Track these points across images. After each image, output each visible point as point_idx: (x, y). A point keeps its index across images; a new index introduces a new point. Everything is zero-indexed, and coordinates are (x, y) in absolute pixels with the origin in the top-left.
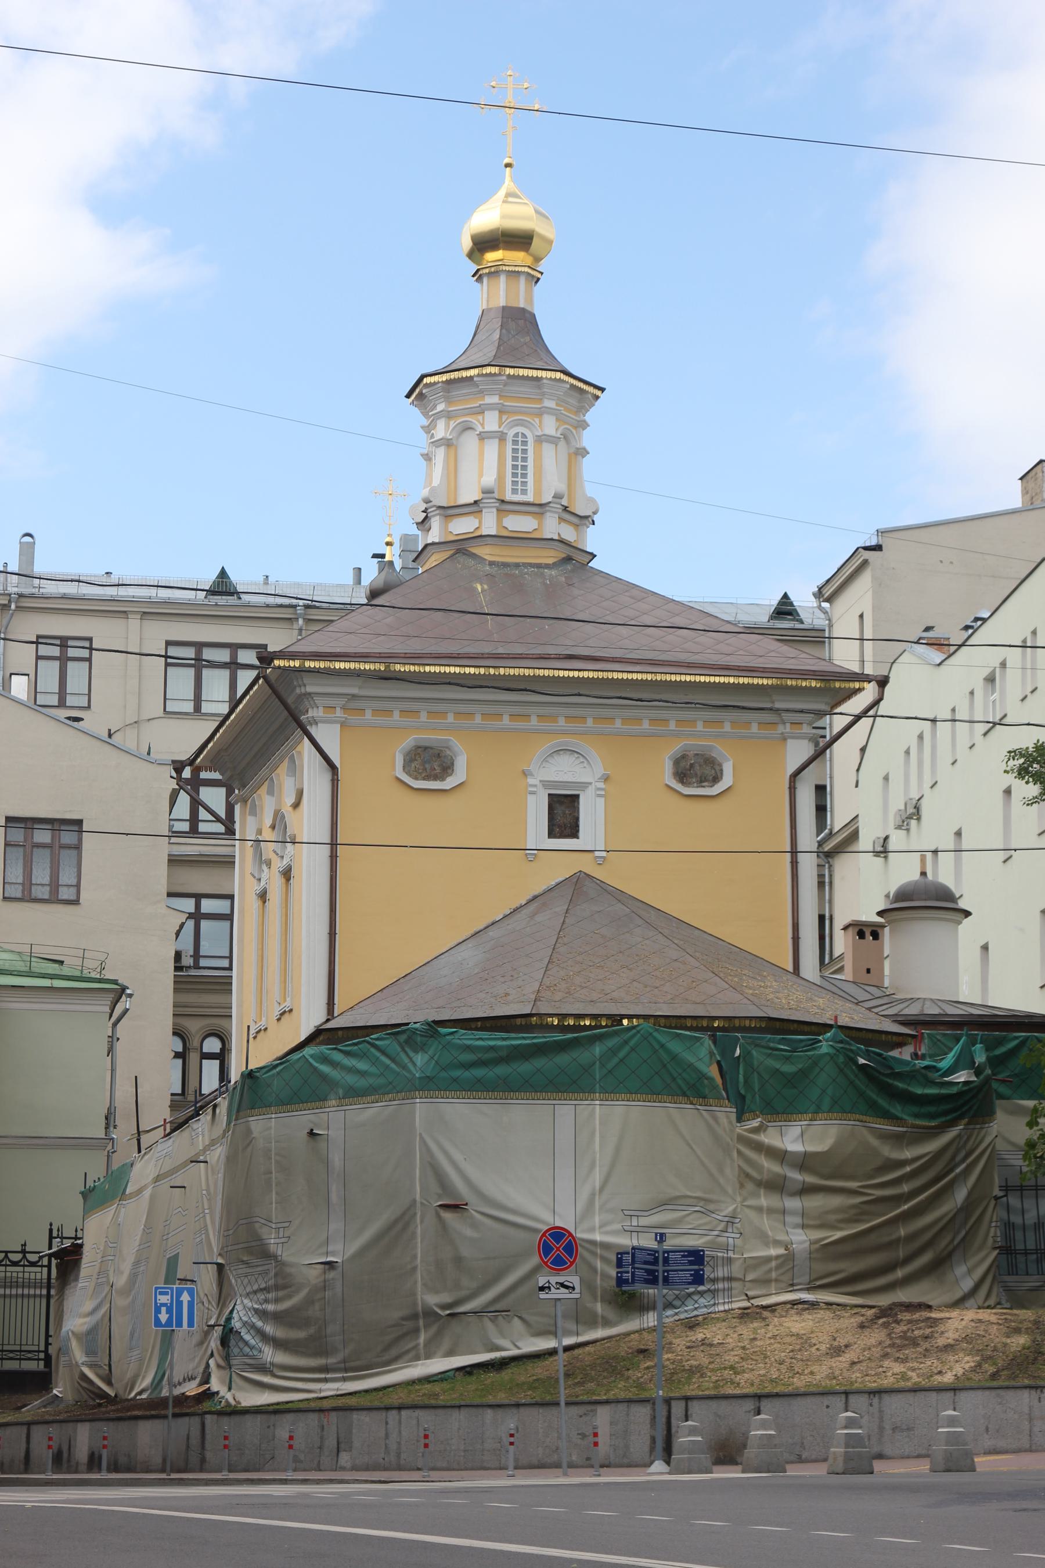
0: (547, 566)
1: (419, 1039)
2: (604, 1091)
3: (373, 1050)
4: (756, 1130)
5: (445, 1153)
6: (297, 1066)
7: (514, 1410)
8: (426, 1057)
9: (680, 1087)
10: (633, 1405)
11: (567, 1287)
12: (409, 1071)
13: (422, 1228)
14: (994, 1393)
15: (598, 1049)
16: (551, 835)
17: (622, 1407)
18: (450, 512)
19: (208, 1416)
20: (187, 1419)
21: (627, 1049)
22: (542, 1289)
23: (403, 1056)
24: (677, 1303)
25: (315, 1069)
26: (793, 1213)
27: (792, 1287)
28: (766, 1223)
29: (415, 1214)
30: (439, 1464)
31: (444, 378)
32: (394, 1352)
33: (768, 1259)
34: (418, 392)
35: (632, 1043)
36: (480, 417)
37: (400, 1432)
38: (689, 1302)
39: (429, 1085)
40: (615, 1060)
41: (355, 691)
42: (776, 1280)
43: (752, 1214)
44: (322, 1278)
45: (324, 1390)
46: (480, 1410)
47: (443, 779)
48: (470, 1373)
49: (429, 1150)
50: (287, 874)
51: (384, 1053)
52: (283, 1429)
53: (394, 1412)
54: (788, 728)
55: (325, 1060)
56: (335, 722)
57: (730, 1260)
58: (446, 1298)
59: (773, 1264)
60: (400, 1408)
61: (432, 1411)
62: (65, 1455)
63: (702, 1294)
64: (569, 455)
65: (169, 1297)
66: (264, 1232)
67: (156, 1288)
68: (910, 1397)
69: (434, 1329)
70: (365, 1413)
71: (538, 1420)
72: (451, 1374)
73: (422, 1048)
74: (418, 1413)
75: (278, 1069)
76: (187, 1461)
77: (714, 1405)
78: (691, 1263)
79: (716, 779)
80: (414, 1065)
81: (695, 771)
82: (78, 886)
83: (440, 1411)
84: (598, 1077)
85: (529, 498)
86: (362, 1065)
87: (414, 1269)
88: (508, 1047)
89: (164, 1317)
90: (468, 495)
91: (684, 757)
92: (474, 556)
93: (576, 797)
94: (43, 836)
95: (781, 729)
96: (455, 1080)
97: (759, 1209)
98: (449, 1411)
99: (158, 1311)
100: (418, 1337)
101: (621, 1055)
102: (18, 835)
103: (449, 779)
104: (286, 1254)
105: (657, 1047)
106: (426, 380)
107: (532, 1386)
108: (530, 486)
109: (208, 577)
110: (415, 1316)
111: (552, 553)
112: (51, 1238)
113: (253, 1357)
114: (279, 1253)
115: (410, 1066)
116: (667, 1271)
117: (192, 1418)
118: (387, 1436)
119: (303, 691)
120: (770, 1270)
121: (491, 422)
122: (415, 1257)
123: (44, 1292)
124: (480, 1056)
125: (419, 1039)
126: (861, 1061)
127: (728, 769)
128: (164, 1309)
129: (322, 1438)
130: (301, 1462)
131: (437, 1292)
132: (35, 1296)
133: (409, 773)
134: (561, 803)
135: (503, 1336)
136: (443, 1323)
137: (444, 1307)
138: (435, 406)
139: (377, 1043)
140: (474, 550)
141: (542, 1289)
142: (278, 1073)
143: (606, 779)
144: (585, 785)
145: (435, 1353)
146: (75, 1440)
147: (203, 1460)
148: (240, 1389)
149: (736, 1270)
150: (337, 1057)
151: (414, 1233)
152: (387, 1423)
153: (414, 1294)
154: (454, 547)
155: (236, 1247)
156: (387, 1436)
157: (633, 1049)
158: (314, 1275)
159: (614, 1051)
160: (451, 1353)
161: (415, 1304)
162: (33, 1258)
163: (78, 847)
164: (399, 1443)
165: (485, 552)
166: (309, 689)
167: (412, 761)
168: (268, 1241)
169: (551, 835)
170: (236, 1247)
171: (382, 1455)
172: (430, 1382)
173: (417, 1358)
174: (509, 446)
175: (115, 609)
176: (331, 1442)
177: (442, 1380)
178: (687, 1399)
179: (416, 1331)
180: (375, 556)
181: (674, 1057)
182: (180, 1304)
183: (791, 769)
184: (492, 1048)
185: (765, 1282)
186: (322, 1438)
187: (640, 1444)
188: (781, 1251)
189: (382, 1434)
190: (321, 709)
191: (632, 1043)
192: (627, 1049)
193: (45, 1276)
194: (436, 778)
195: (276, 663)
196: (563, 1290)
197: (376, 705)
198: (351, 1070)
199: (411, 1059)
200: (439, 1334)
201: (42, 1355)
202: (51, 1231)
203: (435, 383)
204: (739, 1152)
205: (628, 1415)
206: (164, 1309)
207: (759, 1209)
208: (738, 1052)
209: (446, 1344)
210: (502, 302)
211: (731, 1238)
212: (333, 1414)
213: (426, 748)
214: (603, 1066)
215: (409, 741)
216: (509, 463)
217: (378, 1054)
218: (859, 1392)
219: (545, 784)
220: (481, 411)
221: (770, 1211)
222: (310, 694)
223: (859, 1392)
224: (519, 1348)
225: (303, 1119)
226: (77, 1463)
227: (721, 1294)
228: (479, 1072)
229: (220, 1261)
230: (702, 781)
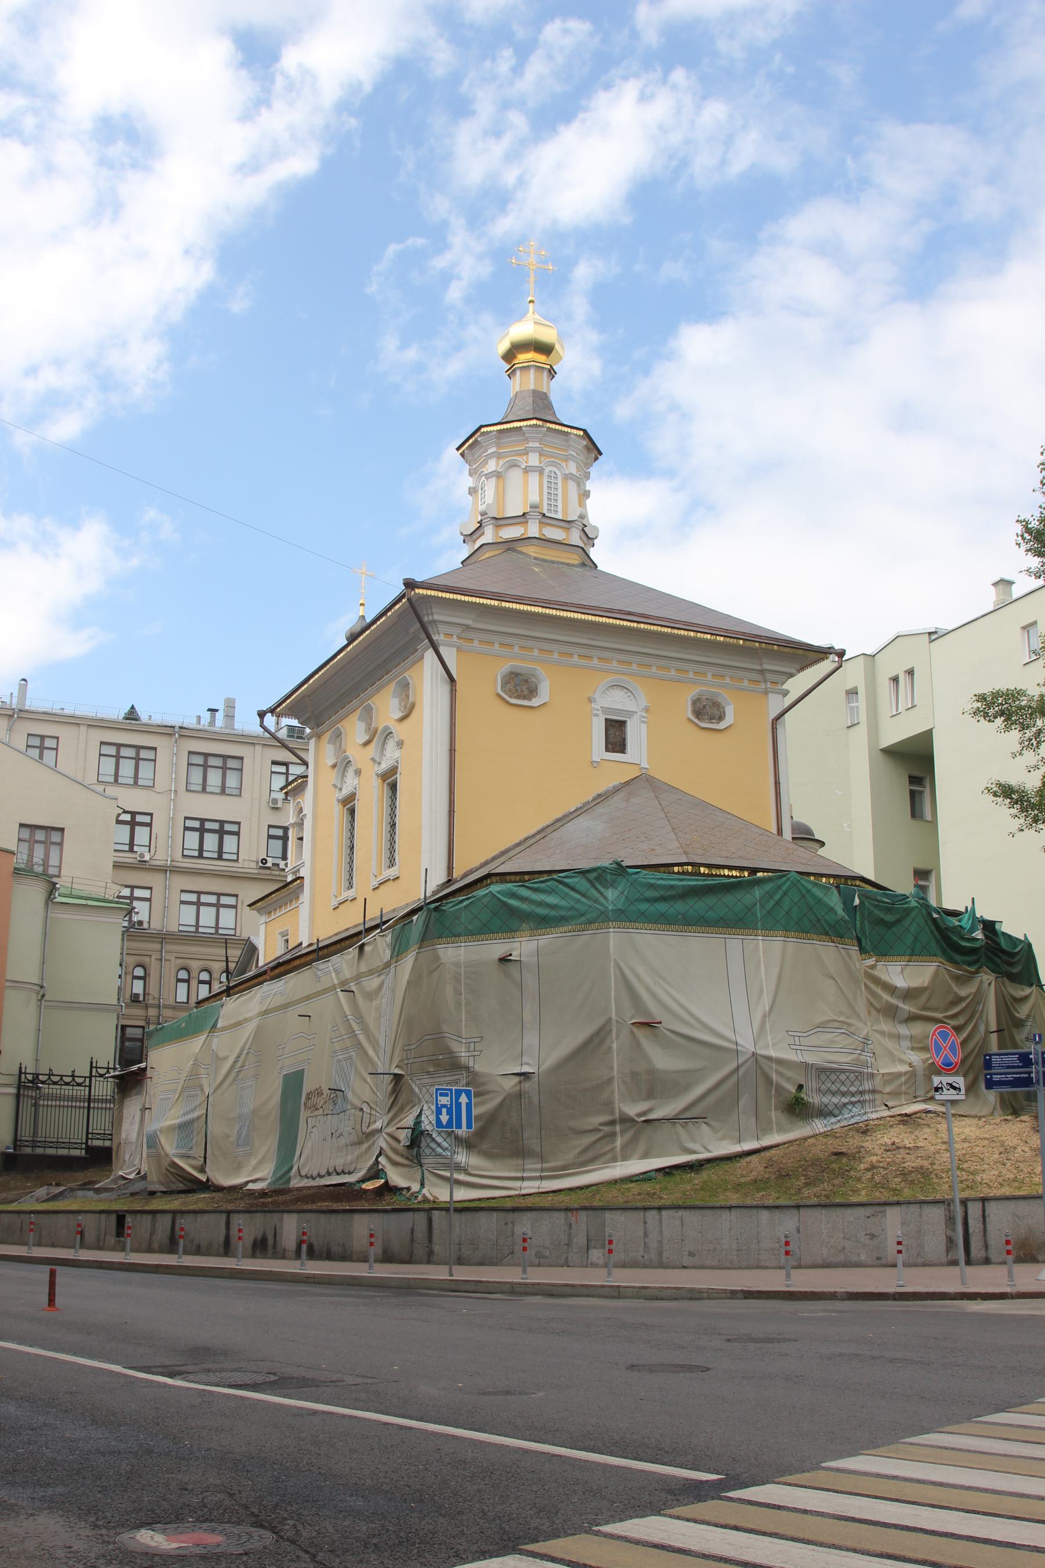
0: (573, 565)
1: (609, 877)
3: (561, 887)
4: (873, 967)
6: (485, 901)
7: (794, 1212)
8: (617, 893)
9: (823, 927)
10: (925, 1206)
11: (955, 1088)
12: (602, 904)
15: (757, 892)
16: (607, 750)
18: (500, 521)
19: (436, 1213)
20: (411, 1214)
21: (781, 893)
22: (937, 1089)
23: (593, 890)
24: (836, 1112)
25: (504, 903)
26: (905, 1037)
27: (915, 1099)
28: (889, 1044)
29: (611, 1030)
30: (708, 1263)
31: (499, 427)
32: (590, 1154)
33: (899, 1075)
35: (785, 888)
36: (525, 457)
37: (661, 1231)
38: (845, 1110)
39: (624, 916)
40: (772, 903)
42: (905, 1093)
43: (879, 1037)
44: (518, 1088)
45: (525, 1188)
46: (754, 1211)
47: (530, 700)
48: (669, 1174)
51: (573, 889)
52: (524, 1225)
53: (654, 1212)
54: (769, 685)
55: (513, 895)
56: (454, 646)
58: (642, 1106)
59: (903, 1079)
60: (660, 1209)
61: (698, 1212)
62: (270, 1242)
63: (853, 1103)
64: (579, 495)
65: (448, 1098)
66: (455, 1046)
67: (437, 1090)
70: (619, 1212)
71: (821, 1222)
72: (653, 1174)
73: (612, 885)
74: (681, 1213)
75: (465, 903)
76: (411, 1253)
79: (721, 718)
80: (605, 898)
81: (707, 711)
82: (60, 867)
83: (709, 1213)
84: (759, 916)
85: (560, 516)
88: (683, 886)
89: (444, 1118)
90: (514, 509)
91: (699, 699)
92: (521, 552)
94: (40, 835)
95: (763, 686)
97: (883, 1033)
98: (719, 1212)
99: (439, 1112)
100: (614, 1142)
101: (777, 897)
102: (26, 834)
103: (534, 700)
105: (804, 892)
106: (483, 430)
107: (738, 1187)
109: (118, 713)
110: (612, 1123)
111: (576, 557)
112: (92, 1067)
114: (471, 1064)
115: (601, 899)
116: (991, 1074)
117: (417, 1214)
118: (646, 1235)
119: (430, 618)
120: (901, 1085)
121: (534, 460)
123: (86, 1105)
124: (662, 893)
125: (609, 877)
126: (935, 916)
127: (730, 711)
128: (444, 1110)
129: (570, 1235)
130: (547, 1257)
131: (634, 1101)
132: (80, 1107)
133: (504, 692)
134: (613, 727)
138: (487, 450)
139: (566, 880)
140: (524, 549)
141: (937, 1089)
142: (466, 907)
143: (647, 710)
144: (631, 714)
145: (631, 1155)
146: (281, 1229)
147: (431, 1253)
148: (434, 1185)
150: (524, 892)
152: (645, 1223)
154: (506, 546)
155: (420, 1059)
156: (646, 1235)
157: (785, 893)
159: (770, 895)
160: (645, 1155)
162: (79, 1080)
163: (61, 844)
164: (660, 1242)
165: (531, 550)
166: (436, 617)
167: (507, 683)
168: (459, 1054)
169: (607, 750)
170: (420, 1059)
171: (642, 1253)
172: (632, 1181)
173: (614, 1160)
174: (546, 479)
176: (580, 1239)
177: (644, 1180)
178: (984, 1200)
179: (613, 1135)
180: (209, 710)
182: (459, 1105)
183: (773, 715)
184: (672, 887)
185: (896, 1094)
186: (570, 1235)
187: (935, 1244)
188: (907, 1068)
189: (641, 1233)
190: (442, 635)
191: (785, 888)
192: (781, 893)
193: (87, 1093)
194: (524, 698)
195: (417, 591)
196: (952, 1091)
198: (541, 904)
199: (602, 894)
201: (84, 1146)
202: (92, 1063)
203: (491, 432)
204: (866, 986)
205: (921, 1216)
206: (444, 1110)
207: (883, 1033)
208: (857, 902)
209: (642, 1147)
210: (532, 387)
211: (867, 1057)
212: (583, 1215)
213: (517, 674)
214: (762, 907)
215: (506, 667)
216: (546, 490)
217: (566, 890)
219: (605, 710)
221: (891, 1036)
222: (435, 621)
224: (709, 1151)
225: (497, 948)
226: (284, 1250)
227: (867, 1104)
228: (662, 907)
229: (398, 1071)
230: (711, 719)
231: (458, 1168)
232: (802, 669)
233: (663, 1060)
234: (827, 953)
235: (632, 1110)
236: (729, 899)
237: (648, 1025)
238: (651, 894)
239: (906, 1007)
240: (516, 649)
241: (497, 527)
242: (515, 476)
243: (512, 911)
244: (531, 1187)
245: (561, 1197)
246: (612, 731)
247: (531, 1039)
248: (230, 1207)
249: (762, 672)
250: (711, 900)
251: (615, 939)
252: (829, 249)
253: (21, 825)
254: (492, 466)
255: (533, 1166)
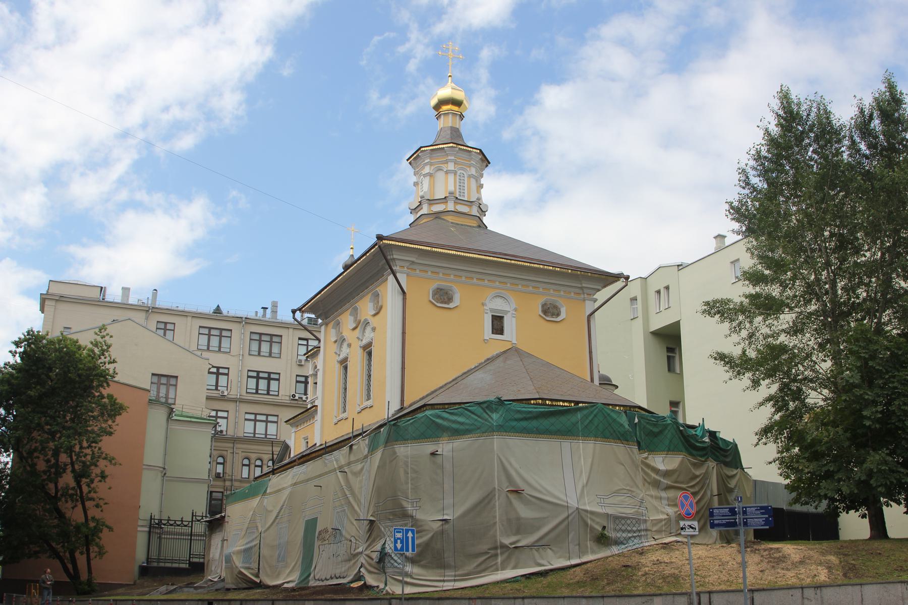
2: (583, 436)
4: (646, 458)
5: (511, 464)
6: (422, 420)
7: (601, 600)
8: (498, 415)
13: (498, 503)
14: (882, 586)
15: (579, 415)
17: (669, 598)
18: (431, 202)
22: (682, 529)
23: (485, 415)
26: (664, 498)
28: (656, 503)
32: (483, 567)
33: (661, 520)
34: (415, 159)
38: (630, 541)
39: (502, 429)
40: (588, 421)
41: (414, 259)
46: (578, 600)
49: (502, 462)
50: (368, 350)
53: (520, 600)
55: (439, 417)
57: (645, 521)
58: (513, 539)
63: (635, 537)
66: (405, 504)
68: (837, 589)
69: (506, 555)
73: (496, 411)
77: (726, 595)
78: (762, 514)
79: (558, 315)
81: (550, 311)
86: (461, 419)
87: (495, 523)
89: (399, 546)
90: (440, 195)
93: (502, 318)
94: (164, 380)
96: (513, 427)
97: (652, 496)
98: (557, 600)
99: (396, 542)
100: (497, 559)
101: (590, 418)
102: (155, 379)
104: (419, 515)
108: (466, 194)
110: (496, 548)
113: (399, 568)
121: (451, 166)
122: (495, 517)
127: (563, 311)
131: (508, 536)
135: (542, 558)
136: (512, 552)
137: (511, 544)
141: (682, 529)
143: (515, 310)
149: (649, 525)
151: (495, 505)
153: (495, 536)
157: (595, 416)
158: (437, 526)
159: (586, 416)
160: (515, 567)
161: (496, 541)
163: (176, 385)
165: (449, 218)
166: (395, 256)
173: (497, 570)
174: (458, 178)
175: (184, 314)
177: (514, 582)
178: (710, 593)
179: (496, 555)
181: (615, 420)
182: (407, 538)
183: (588, 313)
184: (530, 412)
185: (659, 531)
188: (666, 517)
197: (422, 268)
200: (509, 558)
207: (652, 496)
209: (512, 564)
210: (450, 125)
213: (441, 289)
214: (582, 423)
218: (809, 587)
219: (492, 310)
220: (446, 162)
221: (656, 498)
223: (809, 587)
225: (429, 447)
228: (524, 424)
230: (553, 315)
231: (407, 575)
232: (605, 287)
233: (525, 512)
234: (619, 450)
235: (507, 541)
236: (563, 419)
237: (516, 491)
238: (518, 416)
239: (665, 481)
240: (441, 275)
241: (430, 204)
242: (440, 176)
243: (438, 426)
244: (449, 586)
245: (466, 592)
246: (495, 322)
247: (448, 501)
248: (274, 597)
249: (582, 288)
250: (552, 420)
251: (497, 442)
252: (626, 43)
253: (153, 374)
254: (427, 170)
255: (450, 573)
